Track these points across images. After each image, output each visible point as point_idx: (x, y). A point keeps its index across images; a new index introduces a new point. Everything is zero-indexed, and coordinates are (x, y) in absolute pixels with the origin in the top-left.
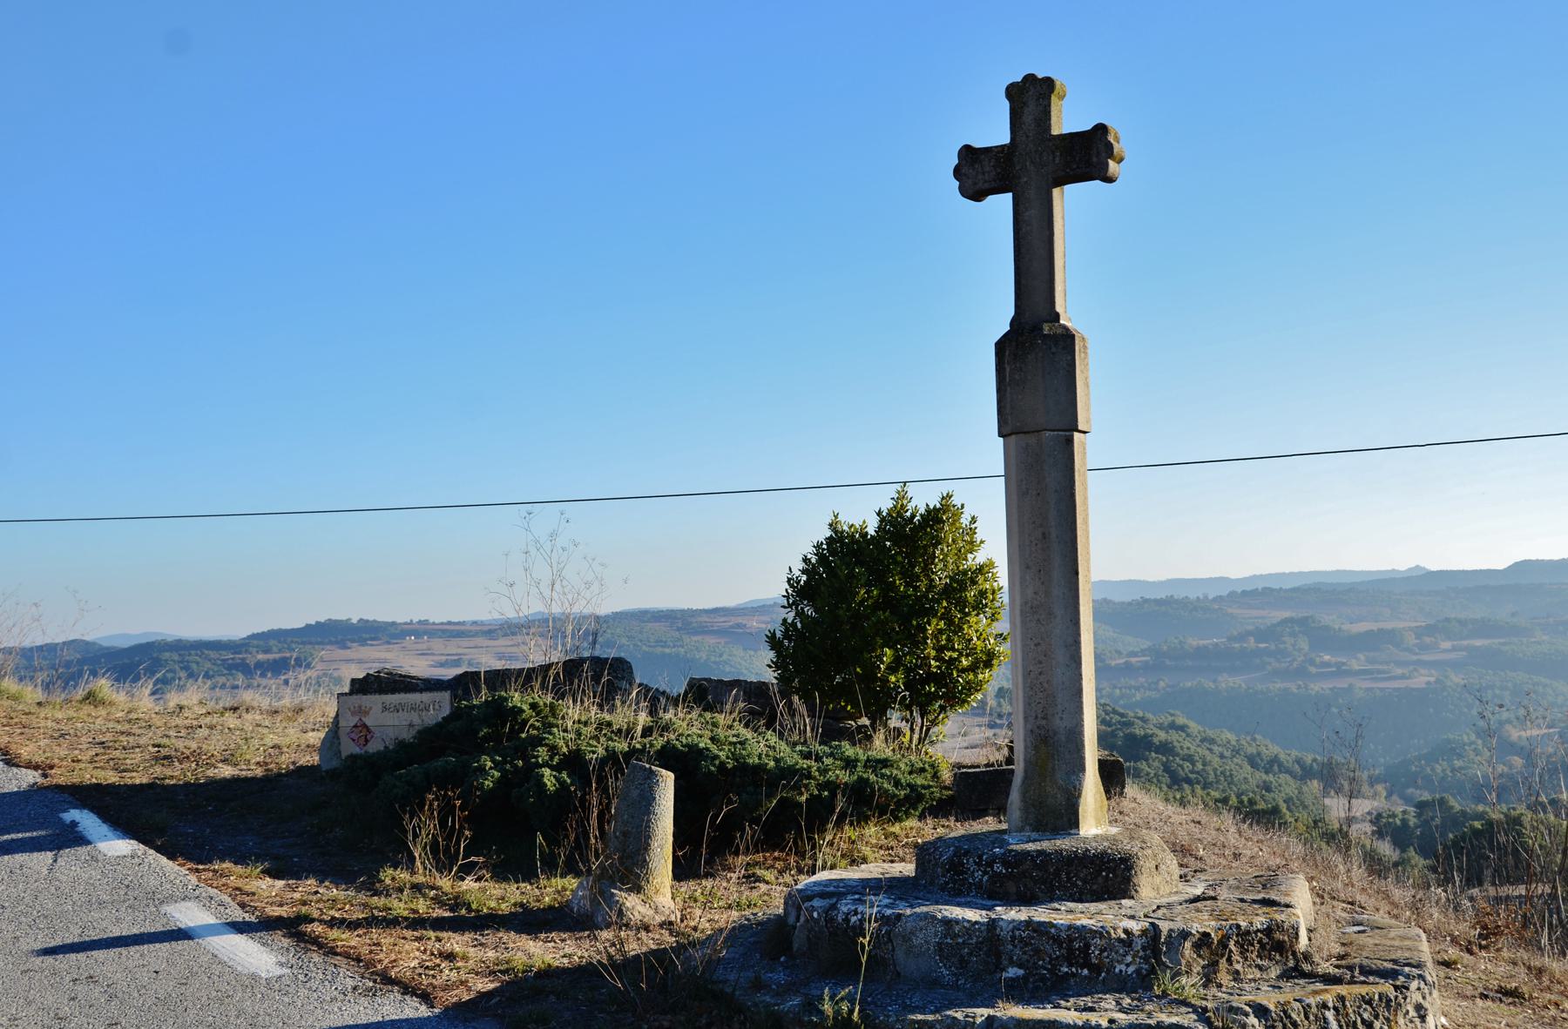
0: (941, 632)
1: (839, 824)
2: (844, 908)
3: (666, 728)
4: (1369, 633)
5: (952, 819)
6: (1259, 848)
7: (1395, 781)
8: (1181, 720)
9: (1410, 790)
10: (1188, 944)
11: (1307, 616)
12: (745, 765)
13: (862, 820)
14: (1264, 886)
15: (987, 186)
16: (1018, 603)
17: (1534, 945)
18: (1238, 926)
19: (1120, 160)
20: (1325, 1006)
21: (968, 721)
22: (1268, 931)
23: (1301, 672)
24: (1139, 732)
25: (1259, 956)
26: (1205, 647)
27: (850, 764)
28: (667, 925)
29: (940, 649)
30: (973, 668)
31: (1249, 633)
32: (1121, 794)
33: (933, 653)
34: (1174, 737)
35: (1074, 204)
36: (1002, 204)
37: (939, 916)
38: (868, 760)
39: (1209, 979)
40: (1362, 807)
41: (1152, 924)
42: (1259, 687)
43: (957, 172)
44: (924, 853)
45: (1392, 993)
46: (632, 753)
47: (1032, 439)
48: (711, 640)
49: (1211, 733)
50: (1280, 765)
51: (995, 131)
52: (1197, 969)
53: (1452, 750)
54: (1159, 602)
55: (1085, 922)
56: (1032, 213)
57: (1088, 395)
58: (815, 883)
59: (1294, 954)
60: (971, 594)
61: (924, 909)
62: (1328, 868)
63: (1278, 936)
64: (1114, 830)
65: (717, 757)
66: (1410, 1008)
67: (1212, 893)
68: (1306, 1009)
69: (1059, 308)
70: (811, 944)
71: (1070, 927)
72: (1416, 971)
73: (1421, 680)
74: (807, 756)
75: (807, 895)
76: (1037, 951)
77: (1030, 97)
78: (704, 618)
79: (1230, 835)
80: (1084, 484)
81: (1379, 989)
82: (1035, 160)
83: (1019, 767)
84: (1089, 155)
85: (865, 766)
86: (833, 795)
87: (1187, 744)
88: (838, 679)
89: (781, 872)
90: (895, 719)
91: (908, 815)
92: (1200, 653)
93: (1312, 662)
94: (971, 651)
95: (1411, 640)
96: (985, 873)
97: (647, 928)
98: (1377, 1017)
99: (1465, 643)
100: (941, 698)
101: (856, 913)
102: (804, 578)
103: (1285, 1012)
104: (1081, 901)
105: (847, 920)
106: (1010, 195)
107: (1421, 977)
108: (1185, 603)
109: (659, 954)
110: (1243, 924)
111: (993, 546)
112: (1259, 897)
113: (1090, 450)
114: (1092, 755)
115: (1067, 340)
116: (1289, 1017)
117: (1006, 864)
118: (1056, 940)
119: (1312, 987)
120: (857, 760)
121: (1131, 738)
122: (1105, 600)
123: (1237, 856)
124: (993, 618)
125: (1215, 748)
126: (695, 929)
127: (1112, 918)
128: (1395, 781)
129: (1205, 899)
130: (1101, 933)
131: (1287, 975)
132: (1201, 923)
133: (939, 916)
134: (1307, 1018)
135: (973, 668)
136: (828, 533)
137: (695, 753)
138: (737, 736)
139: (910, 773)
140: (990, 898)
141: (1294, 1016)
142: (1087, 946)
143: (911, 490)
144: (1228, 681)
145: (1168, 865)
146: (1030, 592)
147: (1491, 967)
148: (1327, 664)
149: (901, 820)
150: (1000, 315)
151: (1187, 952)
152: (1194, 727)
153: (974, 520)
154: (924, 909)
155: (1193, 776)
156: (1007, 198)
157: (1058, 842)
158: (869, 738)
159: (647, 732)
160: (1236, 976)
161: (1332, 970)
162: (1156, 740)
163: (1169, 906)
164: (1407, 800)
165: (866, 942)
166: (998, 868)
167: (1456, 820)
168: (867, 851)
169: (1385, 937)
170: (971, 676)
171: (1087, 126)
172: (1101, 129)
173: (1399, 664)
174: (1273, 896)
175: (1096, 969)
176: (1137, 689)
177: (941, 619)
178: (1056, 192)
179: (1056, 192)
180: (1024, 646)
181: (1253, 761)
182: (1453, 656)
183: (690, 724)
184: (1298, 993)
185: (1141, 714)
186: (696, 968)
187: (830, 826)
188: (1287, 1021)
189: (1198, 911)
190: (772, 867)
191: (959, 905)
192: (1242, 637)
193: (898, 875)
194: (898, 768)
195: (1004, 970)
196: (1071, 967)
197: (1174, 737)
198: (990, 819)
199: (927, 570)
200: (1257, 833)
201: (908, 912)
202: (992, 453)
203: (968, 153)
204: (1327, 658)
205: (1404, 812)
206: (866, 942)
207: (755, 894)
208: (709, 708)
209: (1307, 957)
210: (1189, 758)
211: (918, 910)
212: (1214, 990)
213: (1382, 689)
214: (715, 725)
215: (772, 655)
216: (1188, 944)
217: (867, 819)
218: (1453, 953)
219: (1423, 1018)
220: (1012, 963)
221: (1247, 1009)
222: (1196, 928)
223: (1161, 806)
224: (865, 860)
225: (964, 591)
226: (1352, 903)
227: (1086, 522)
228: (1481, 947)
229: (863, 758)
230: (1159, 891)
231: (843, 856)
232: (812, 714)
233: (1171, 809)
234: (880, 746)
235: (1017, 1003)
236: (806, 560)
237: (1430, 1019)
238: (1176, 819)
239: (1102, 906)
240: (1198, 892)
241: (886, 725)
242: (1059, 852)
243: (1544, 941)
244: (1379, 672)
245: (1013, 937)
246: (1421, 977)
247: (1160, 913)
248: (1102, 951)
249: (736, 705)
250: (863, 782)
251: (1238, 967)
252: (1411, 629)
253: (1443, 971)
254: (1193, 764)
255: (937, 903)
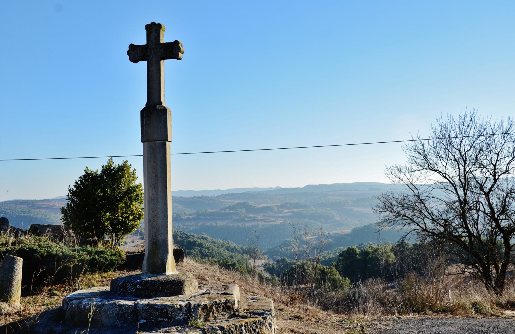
0: (123, 208)
1: (85, 274)
2: (84, 303)
3: (21, 242)
4: (264, 207)
5: (125, 271)
6: (225, 276)
7: (271, 254)
8: (205, 236)
9: (275, 257)
10: (200, 309)
11: (244, 203)
12: (472, 265)
13: (93, 272)
14: (225, 289)
15: (138, 58)
16: (147, 198)
17: (305, 302)
18: (216, 302)
19: (183, 53)
20: (242, 325)
21: (135, 237)
22: (225, 303)
23: (243, 220)
24: (192, 240)
25: (222, 311)
26: (213, 212)
27: (89, 253)
28: (18, 313)
29: (123, 213)
30: (134, 220)
31: (227, 208)
32: (182, 260)
33: (120, 215)
34: (203, 241)
35: (167, 66)
36: (143, 65)
37: (118, 304)
38: (96, 251)
39: (206, 319)
40: (259, 262)
41: (189, 303)
42: (230, 225)
43: (128, 53)
44: (114, 283)
45: (262, 320)
46: (7, 251)
47: (152, 144)
48: (42, 211)
49: (214, 240)
50: (236, 250)
51: (142, 40)
52: (203, 316)
53: (286, 244)
54: (199, 198)
55: (167, 303)
56: (153, 68)
57: (171, 129)
58: (74, 295)
59: (233, 310)
60: (133, 195)
61: (112, 302)
62: (247, 282)
63: (229, 304)
64: (178, 273)
65: (40, 252)
66: (267, 324)
67: (208, 292)
68: (236, 327)
69: (162, 100)
70: (67, 317)
71: (162, 305)
72: (269, 313)
73: (279, 222)
74: (74, 251)
75: (71, 299)
76: (151, 314)
77: (153, 30)
78: (40, 203)
79: (217, 273)
80: (170, 159)
81: (258, 319)
82: (154, 51)
83: (146, 253)
84: (173, 50)
85: (95, 254)
86: (83, 264)
87: (207, 244)
88: (86, 224)
89: (63, 292)
90: (107, 238)
91: (110, 270)
92: (212, 214)
93: (246, 217)
94: (133, 214)
95: (276, 209)
96: (134, 288)
97: (10, 315)
98: (257, 328)
99: (291, 210)
100: (122, 230)
101: (88, 304)
102: (75, 189)
103: (229, 328)
104: (166, 296)
105: (85, 307)
106: (146, 62)
107: (271, 314)
108: (207, 198)
109: (13, 324)
110: (218, 301)
111: (140, 180)
112: (223, 292)
113: (171, 148)
114: (171, 247)
115: (164, 111)
116: (231, 330)
117: (141, 285)
118: (157, 310)
119: (238, 320)
120: (92, 252)
121: (189, 242)
122: (181, 197)
123: (219, 279)
124: (141, 203)
125: (216, 245)
126: (29, 314)
127: (176, 301)
128: (271, 254)
129: (206, 294)
130: (172, 307)
131: (231, 317)
132: (205, 301)
133: (118, 304)
134: (236, 330)
135: (134, 220)
136: (84, 173)
137: (32, 251)
138: (48, 244)
139: (111, 256)
140: (135, 297)
141: (232, 329)
142: (167, 311)
143: (114, 159)
144: (221, 223)
145: (194, 281)
146: (151, 194)
147: (292, 310)
148: (251, 217)
149: (107, 272)
150: (142, 102)
151: (200, 311)
152: (209, 238)
153: (135, 170)
154: (112, 302)
155: (208, 254)
156: (145, 63)
157: (159, 277)
158: (97, 244)
159: (13, 244)
160: (215, 318)
161: (245, 314)
162: (197, 243)
163: (195, 296)
164: (274, 260)
165: (91, 314)
166: (138, 286)
167: (287, 265)
168: (95, 283)
169: (261, 303)
170: (133, 223)
171: (172, 41)
172: (176, 42)
173: (272, 217)
174: (227, 292)
175: (170, 319)
176: (191, 226)
177: (124, 203)
178: (162, 62)
179: (162, 62)
180: (149, 212)
181: (227, 249)
182: (288, 214)
183: (30, 241)
184: (234, 322)
185: (192, 234)
186: (27, 328)
187: (81, 275)
188: (230, 331)
189: (204, 297)
190: (60, 290)
191: (125, 300)
192: (225, 209)
193: (104, 290)
194: (107, 254)
195: (139, 321)
196: (164, 317)
197: (203, 241)
198: (138, 270)
199: (119, 187)
200: (225, 271)
201: (107, 303)
202: (139, 147)
203: (132, 46)
204: (251, 215)
205: (273, 263)
206: (91, 314)
207: (53, 300)
208: (38, 235)
209: (237, 310)
210: (208, 248)
211: (110, 302)
212: (208, 323)
213: (267, 225)
214: (40, 241)
215: (62, 215)
216: (200, 309)
217: (95, 272)
218: (282, 306)
219: (271, 327)
220: (142, 318)
221: (218, 328)
222: (203, 303)
223: (195, 264)
224: (93, 286)
225: (131, 193)
226: (253, 293)
227: (170, 171)
228: (291, 304)
229: (94, 251)
230: (192, 292)
231: (86, 285)
232: (77, 236)
233: (198, 265)
234: (101, 247)
235: (143, 332)
236: (76, 182)
237: (273, 327)
238: (200, 268)
239: (173, 298)
240: (204, 292)
241: (103, 239)
242: (159, 281)
243: (308, 301)
244: (266, 220)
245: (143, 310)
246: (271, 314)
247: (191, 299)
248: (172, 312)
249: (48, 233)
250: (94, 259)
251: (216, 315)
252: (276, 206)
253: (279, 312)
254: (209, 250)
255: (117, 300)
